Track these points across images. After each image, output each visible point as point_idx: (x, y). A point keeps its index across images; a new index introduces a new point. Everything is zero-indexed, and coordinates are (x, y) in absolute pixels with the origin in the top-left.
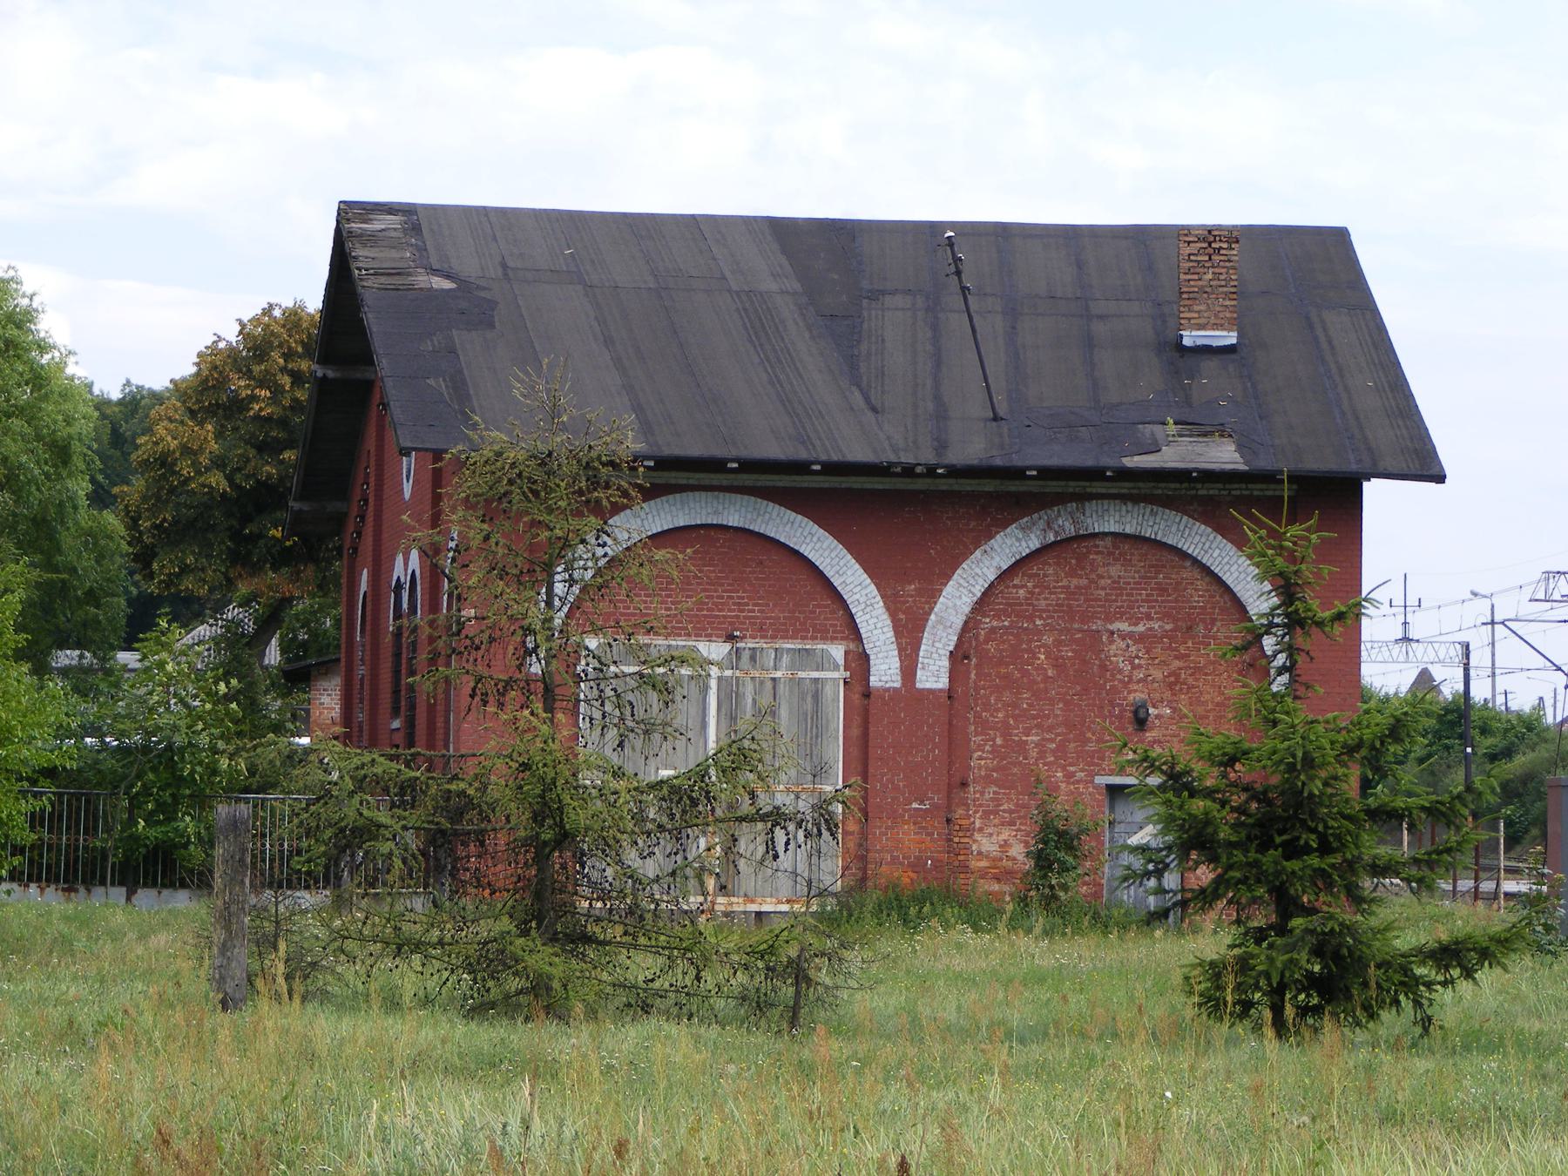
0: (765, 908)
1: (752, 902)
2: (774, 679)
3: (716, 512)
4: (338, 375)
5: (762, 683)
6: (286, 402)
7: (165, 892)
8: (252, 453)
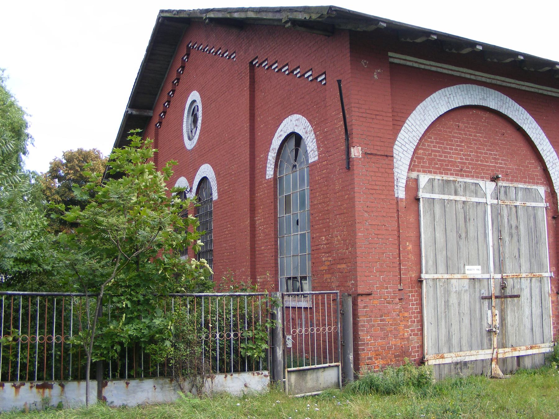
0: (522, 353)
1: (515, 350)
2: (516, 206)
3: (484, 99)
4: (138, 113)
5: (511, 208)
6: (78, 175)
7: (133, 383)
8: (67, 190)
